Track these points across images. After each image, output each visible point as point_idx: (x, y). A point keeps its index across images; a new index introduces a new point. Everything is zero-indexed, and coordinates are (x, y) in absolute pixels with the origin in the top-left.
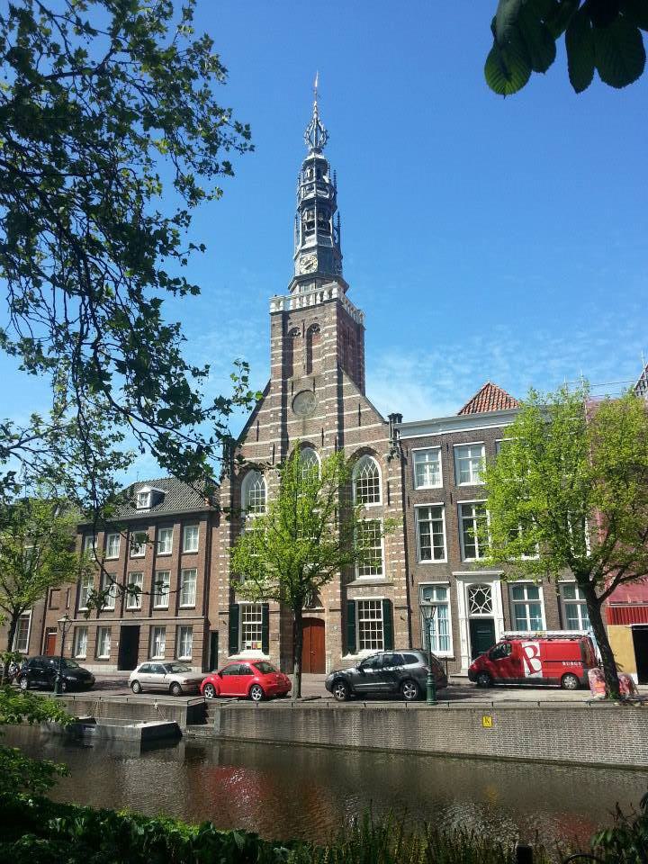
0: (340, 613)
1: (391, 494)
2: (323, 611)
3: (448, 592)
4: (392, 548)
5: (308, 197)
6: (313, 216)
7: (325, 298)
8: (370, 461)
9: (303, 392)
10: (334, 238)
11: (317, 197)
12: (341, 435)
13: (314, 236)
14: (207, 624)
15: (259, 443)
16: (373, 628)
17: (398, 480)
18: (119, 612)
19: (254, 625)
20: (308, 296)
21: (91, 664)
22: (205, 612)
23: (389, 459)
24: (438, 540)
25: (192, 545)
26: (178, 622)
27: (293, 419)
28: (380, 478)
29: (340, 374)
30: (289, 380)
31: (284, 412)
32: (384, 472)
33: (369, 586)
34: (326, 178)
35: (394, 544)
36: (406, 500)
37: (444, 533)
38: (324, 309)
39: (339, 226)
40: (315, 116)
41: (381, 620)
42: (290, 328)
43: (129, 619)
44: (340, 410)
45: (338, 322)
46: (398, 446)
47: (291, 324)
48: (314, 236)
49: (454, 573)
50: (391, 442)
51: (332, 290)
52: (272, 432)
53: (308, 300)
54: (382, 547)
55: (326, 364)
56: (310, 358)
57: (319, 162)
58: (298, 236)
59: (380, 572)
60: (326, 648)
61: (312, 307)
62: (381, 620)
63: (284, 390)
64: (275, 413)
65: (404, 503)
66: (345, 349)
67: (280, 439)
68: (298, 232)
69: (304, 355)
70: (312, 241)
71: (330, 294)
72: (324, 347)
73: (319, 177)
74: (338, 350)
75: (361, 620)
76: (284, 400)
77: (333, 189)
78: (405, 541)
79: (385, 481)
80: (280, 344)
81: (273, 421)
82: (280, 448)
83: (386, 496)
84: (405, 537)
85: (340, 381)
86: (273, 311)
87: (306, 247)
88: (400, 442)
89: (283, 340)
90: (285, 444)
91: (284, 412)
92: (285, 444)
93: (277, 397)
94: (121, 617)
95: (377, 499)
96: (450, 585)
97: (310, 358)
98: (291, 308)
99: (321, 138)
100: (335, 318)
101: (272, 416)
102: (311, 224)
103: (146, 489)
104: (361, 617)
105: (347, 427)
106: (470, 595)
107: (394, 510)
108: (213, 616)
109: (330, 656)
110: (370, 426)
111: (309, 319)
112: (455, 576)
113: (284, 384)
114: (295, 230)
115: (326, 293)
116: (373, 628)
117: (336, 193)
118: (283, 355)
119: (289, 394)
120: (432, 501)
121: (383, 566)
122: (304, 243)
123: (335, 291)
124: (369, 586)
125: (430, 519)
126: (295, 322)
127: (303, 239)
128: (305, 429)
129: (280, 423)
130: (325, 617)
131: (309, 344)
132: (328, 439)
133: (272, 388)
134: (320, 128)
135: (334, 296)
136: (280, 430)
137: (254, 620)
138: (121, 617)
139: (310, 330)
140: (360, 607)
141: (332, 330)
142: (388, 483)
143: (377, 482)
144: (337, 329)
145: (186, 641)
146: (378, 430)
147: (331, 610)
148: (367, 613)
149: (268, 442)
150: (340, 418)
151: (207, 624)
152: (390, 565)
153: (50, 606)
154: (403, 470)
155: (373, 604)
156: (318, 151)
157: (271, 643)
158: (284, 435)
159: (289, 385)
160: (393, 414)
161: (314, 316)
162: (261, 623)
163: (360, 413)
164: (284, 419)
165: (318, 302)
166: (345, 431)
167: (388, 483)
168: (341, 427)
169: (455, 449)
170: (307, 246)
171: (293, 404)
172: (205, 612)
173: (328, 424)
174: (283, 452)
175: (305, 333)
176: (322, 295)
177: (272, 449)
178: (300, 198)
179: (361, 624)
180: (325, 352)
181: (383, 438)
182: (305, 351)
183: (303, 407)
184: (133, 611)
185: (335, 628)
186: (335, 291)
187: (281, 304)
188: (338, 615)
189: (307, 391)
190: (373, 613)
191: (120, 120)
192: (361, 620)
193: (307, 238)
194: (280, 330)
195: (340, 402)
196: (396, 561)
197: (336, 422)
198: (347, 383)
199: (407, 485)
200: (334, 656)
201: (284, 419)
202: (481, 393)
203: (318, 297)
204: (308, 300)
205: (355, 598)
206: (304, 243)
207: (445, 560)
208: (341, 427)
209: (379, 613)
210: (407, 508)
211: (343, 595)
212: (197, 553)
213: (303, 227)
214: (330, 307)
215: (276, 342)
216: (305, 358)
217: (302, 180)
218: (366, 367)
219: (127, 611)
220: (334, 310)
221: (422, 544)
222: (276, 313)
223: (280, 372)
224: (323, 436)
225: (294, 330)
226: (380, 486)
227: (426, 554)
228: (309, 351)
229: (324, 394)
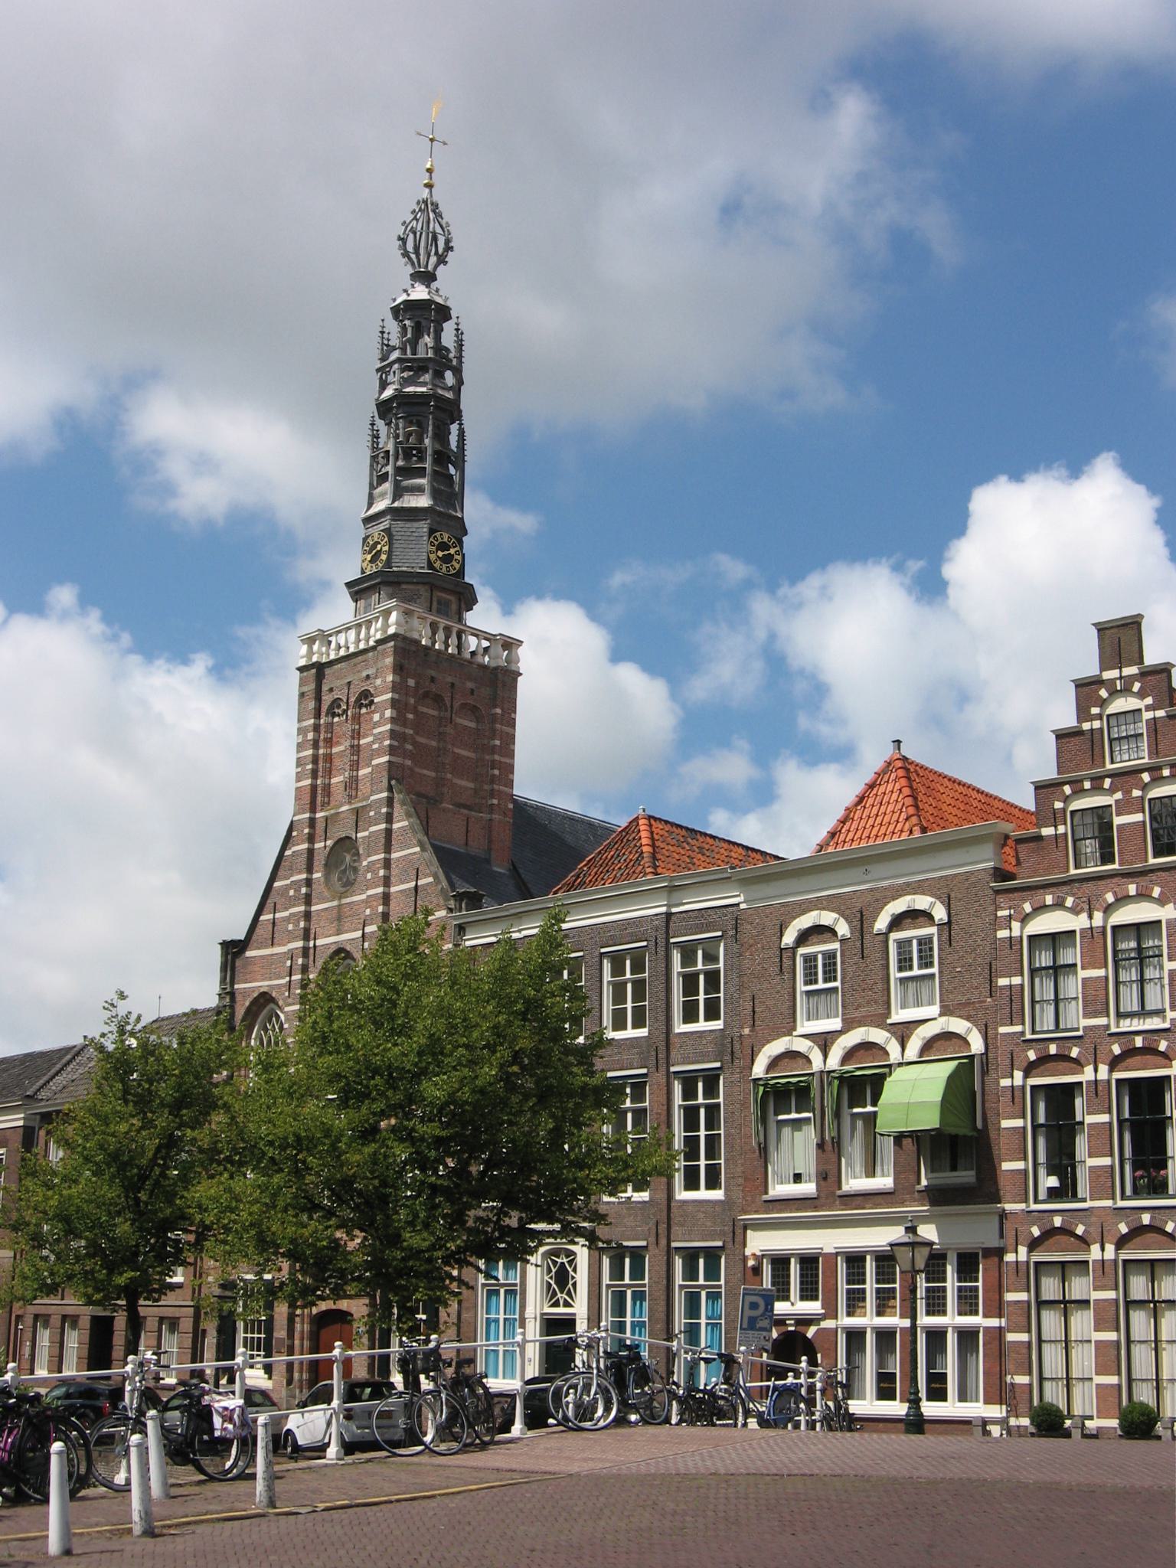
159: (320, 827)
161: (364, 674)
214: (384, 654)
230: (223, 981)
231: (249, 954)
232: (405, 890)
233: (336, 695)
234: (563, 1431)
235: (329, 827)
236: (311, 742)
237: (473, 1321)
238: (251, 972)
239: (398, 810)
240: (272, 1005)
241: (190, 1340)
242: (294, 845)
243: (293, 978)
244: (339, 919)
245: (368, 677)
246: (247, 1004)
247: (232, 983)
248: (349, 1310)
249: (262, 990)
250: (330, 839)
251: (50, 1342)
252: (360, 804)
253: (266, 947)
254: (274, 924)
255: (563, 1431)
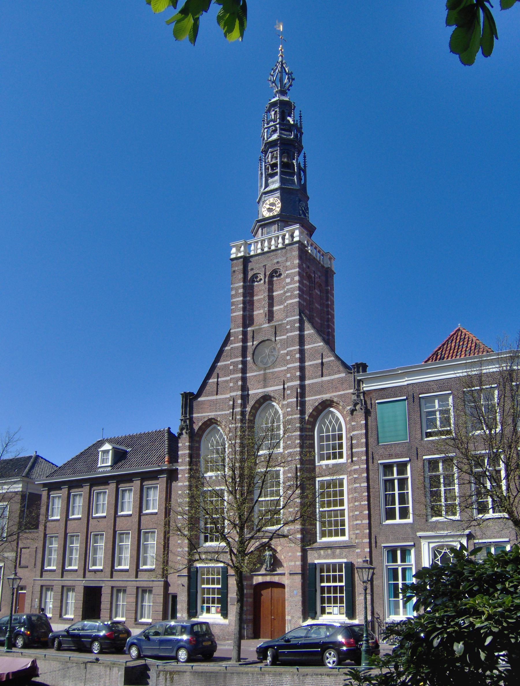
0: (300, 576)
1: (354, 450)
2: (284, 574)
3: (413, 551)
4: (355, 508)
5: (270, 139)
6: (276, 158)
7: (287, 242)
8: (332, 412)
9: (263, 341)
10: (299, 179)
11: (280, 138)
12: (302, 387)
13: (277, 178)
14: (167, 585)
15: (219, 397)
16: (335, 592)
17: (361, 434)
18: (81, 572)
19: (214, 589)
20: (270, 239)
21: (56, 623)
22: (165, 575)
23: (352, 412)
24: (403, 499)
25: (126, 506)
26: (139, 584)
27: (253, 371)
28: (344, 432)
29: (301, 321)
30: (249, 329)
31: (244, 363)
32: (348, 426)
33: (330, 548)
34: (291, 120)
35: (356, 504)
36: (370, 456)
37: (410, 491)
38: (286, 253)
39: (305, 167)
40: (280, 59)
41: (343, 584)
42: (250, 274)
43: (92, 580)
44: (302, 360)
45: (300, 266)
46: (362, 397)
47: (252, 269)
48: (277, 178)
49: (419, 534)
50: (354, 394)
51: (293, 233)
52: (231, 385)
53: (269, 243)
54: (346, 507)
55: (287, 312)
56: (271, 305)
57: (282, 103)
58: (261, 179)
59: (343, 534)
60: (286, 613)
61: (273, 251)
62: (343, 584)
63: (245, 340)
64: (235, 364)
65: (367, 460)
66: (311, 295)
67: (239, 393)
68: (262, 174)
69: (266, 302)
70: (275, 183)
71: (292, 236)
72: (285, 293)
73: (283, 118)
74: (300, 296)
75: (322, 584)
76: (244, 349)
77: (298, 128)
78: (369, 500)
79: (348, 436)
80: (241, 291)
81: (233, 374)
82: (239, 401)
83: (349, 452)
84: (369, 496)
85: (301, 329)
86: (233, 256)
87: (268, 189)
88: (364, 393)
89: (244, 287)
90: (245, 398)
91: (244, 363)
92: (245, 398)
93: (237, 348)
94: (84, 577)
95: (341, 456)
96: (414, 545)
97: (271, 305)
98: (252, 253)
99: (286, 81)
100: (297, 261)
101: (231, 367)
102: (274, 166)
103: (107, 447)
104: (322, 581)
105: (309, 379)
106: (435, 556)
107: (357, 467)
108: (172, 578)
109: (290, 621)
110: (333, 377)
111: (271, 265)
112: (420, 537)
113: (245, 333)
114: (259, 173)
115: (287, 236)
116: (335, 592)
117: (301, 134)
118: (244, 303)
119: (250, 344)
120: (397, 456)
121: (346, 527)
122: (267, 186)
123: (297, 233)
124: (330, 548)
125: (395, 475)
126: (255, 267)
127: (266, 180)
128: (265, 381)
129: (240, 375)
130: (285, 580)
131: (271, 290)
132: (289, 392)
133: (232, 338)
134: (285, 71)
135: (296, 239)
136: (240, 383)
137: (213, 583)
138: (84, 577)
139: (271, 276)
140: (322, 571)
141: (293, 274)
142: (352, 438)
143: (340, 437)
144: (300, 274)
145: (146, 604)
146: (341, 381)
147: (290, 574)
148: (328, 577)
149: (228, 396)
150: (302, 369)
151: (167, 585)
152: (353, 526)
153: (20, 564)
154: (366, 425)
155: (334, 567)
156: (283, 92)
157: (230, 607)
158: (244, 388)
159: (250, 336)
160: (357, 364)
161: (275, 261)
162: (220, 586)
163: (322, 363)
164: (244, 371)
165: (280, 246)
166: (307, 382)
167: (352, 438)
168: (302, 378)
169: (423, 401)
170: (272, 187)
171: (253, 354)
172: (165, 575)
173: (289, 375)
174: (244, 405)
175: (267, 280)
176: (283, 239)
177: (231, 403)
178: (264, 139)
179: (323, 588)
180: (287, 298)
181: (347, 389)
182: (267, 298)
183: (265, 357)
184: (95, 571)
185: (295, 592)
186: (297, 233)
187: (242, 248)
188: (298, 579)
189: (268, 340)
190: (334, 577)
191: (310, 312)
192: (322, 584)
193: (270, 180)
194: (241, 276)
195: (302, 352)
196: (359, 522)
197: (298, 374)
198: (309, 331)
199: (371, 440)
200: (293, 621)
201: (244, 371)
202: (451, 339)
203: (280, 240)
204: (269, 243)
205: (316, 562)
206: (267, 186)
207: (410, 520)
208: (302, 378)
209: (341, 576)
210: (370, 464)
211: (304, 558)
212: (156, 514)
213: (267, 169)
214: (291, 250)
215: (237, 289)
216: (267, 306)
217: (266, 122)
218: (336, 327)
219: (90, 571)
220: (296, 253)
221: (431, 486)
222: (236, 259)
223: (240, 321)
224: (284, 388)
225: (255, 276)
226: (344, 441)
227: (390, 515)
228: (271, 298)
229: (287, 343)
230: (184, 413)
231: (200, 399)
232: (313, 365)
233: (255, 272)
234: (3, 446)
235: (255, 335)
236: (242, 294)
237: (381, 585)
238: (202, 408)
239: (307, 325)
240: (214, 425)
241: (162, 599)
242: (232, 344)
243: (235, 410)
244: (265, 380)
245: (278, 262)
246: (200, 424)
247: (191, 412)
248: (280, 582)
249: (210, 417)
250: (255, 341)
251: (54, 600)
252: (277, 323)
253: (213, 395)
254: (218, 384)
255: (3, 446)
